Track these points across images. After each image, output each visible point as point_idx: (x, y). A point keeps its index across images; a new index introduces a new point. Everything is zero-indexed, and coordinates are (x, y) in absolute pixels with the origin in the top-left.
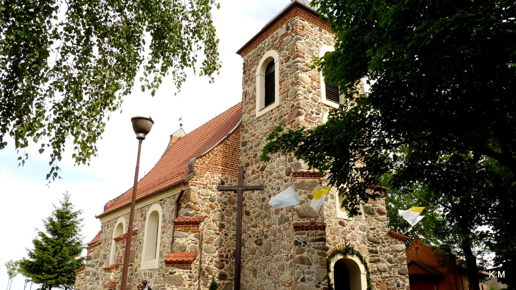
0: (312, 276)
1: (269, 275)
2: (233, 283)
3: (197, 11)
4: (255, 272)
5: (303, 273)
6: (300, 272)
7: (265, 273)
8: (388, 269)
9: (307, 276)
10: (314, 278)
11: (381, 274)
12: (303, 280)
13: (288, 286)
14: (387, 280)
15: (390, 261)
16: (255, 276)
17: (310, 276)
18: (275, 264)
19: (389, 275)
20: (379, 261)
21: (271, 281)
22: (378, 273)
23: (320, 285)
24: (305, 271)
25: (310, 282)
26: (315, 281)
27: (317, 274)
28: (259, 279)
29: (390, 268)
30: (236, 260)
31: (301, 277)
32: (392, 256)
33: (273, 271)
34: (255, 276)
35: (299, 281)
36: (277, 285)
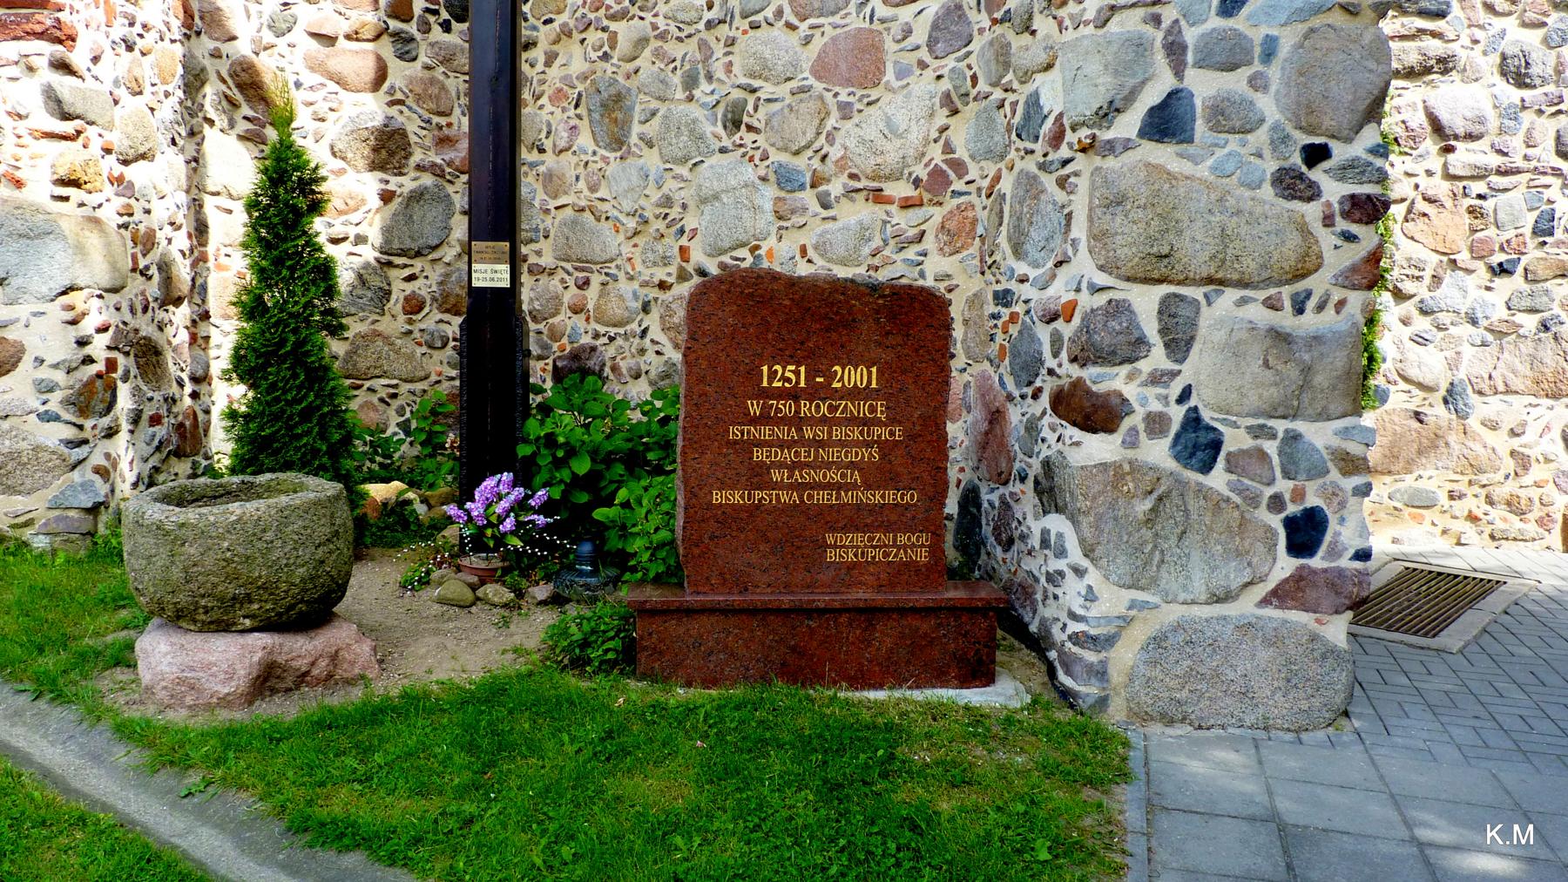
0: (1258, 83)
1: (734, 122)
2: (458, 194)
3: (425, 90)
4: (611, 113)
5: (1175, 50)
6: (1140, 46)
7: (695, 111)
8: (1493, 123)
9: (1203, 85)
10: (1268, 106)
11: (1449, 150)
12: (1166, 123)
13: (907, 204)
14: (1478, 187)
15: (1518, 76)
16: (618, 142)
17: (1236, 82)
18: (794, 39)
19: (1495, 161)
20: (1445, 65)
21: (749, 173)
22: (1430, 145)
23: (1317, 174)
24: (1191, 35)
25: (1233, 142)
26: (1280, 140)
27: (1303, 72)
28: (652, 160)
29: (1512, 114)
30: (472, 38)
31: (1152, 96)
32: (1533, 38)
33: (767, 90)
34: (618, 142)
35: (1128, 125)
36: (808, 197)
